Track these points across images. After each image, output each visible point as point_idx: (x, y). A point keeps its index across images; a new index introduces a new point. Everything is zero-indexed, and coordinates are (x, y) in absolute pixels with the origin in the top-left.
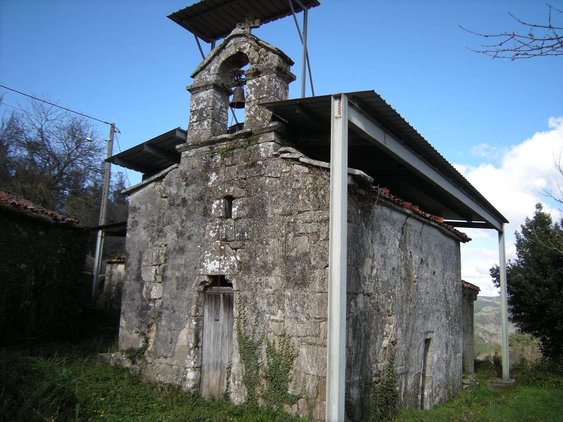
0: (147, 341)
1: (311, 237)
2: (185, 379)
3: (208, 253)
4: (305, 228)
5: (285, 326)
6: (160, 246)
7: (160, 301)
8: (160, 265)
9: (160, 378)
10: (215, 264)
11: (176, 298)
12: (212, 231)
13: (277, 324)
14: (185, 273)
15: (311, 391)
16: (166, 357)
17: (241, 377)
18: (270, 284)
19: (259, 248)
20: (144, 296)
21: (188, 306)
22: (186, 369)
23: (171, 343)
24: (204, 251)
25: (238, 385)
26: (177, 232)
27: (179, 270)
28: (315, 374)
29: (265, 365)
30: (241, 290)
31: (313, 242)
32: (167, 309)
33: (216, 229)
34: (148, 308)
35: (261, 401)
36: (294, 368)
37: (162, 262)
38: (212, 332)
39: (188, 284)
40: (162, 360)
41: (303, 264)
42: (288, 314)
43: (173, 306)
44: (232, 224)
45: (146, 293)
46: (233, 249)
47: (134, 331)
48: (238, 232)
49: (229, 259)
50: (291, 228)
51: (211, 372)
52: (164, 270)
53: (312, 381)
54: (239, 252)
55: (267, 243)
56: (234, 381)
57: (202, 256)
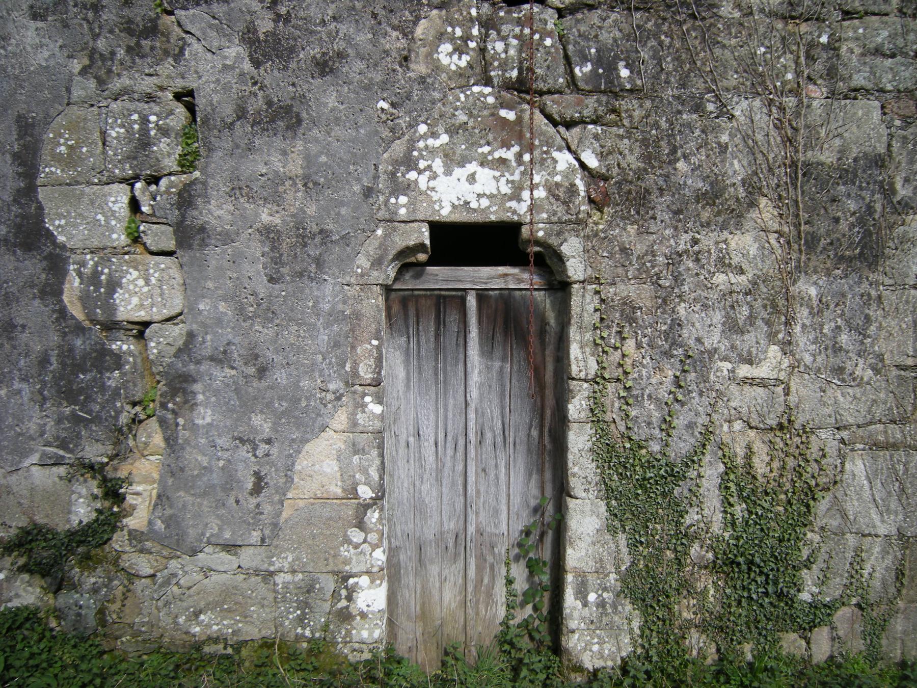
0: (113, 493)
1: (893, 105)
2: (345, 616)
3: (434, 135)
4: (873, 73)
5: (793, 399)
6: (150, 98)
7: (176, 332)
8: (154, 180)
9: (209, 624)
10: (472, 178)
11: (268, 314)
12: (447, 47)
13: (760, 391)
14: (312, 210)
15: (877, 583)
16: (231, 548)
17: (613, 576)
18: (736, 260)
19: (689, 126)
20: (77, 312)
21: (337, 345)
22: (346, 578)
23: (257, 489)
24: (412, 125)
25: (601, 604)
26: (250, 37)
27: (276, 199)
28: (894, 531)
29: (716, 528)
30: (606, 276)
31: (898, 123)
32: (221, 359)
33: (466, 38)
34: (103, 359)
35: (696, 641)
36: (818, 523)
37: (171, 163)
38: (428, 432)
39: (329, 258)
40: (210, 557)
41: (867, 195)
42: (808, 359)
43: (252, 347)
44: (550, 26)
45: (85, 299)
46: (555, 124)
47: (35, 458)
48: (585, 59)
49: (546, 162)
50: (819, 66)
51: (434, 569)
52: (186, 199)
53: (885, 552)
54: (596, 137)
55: (724, 112)
56: (582, 594)
57: (399, 148)
